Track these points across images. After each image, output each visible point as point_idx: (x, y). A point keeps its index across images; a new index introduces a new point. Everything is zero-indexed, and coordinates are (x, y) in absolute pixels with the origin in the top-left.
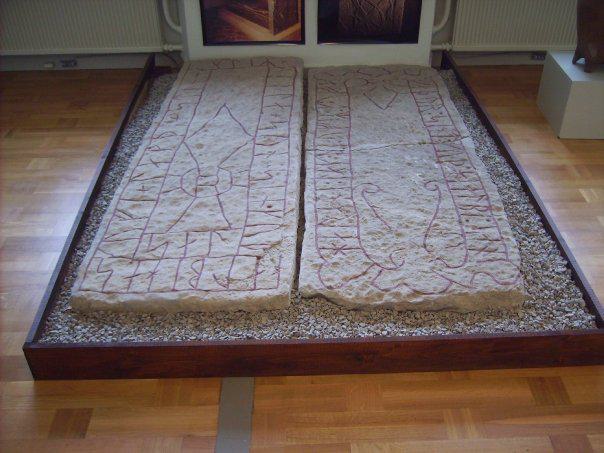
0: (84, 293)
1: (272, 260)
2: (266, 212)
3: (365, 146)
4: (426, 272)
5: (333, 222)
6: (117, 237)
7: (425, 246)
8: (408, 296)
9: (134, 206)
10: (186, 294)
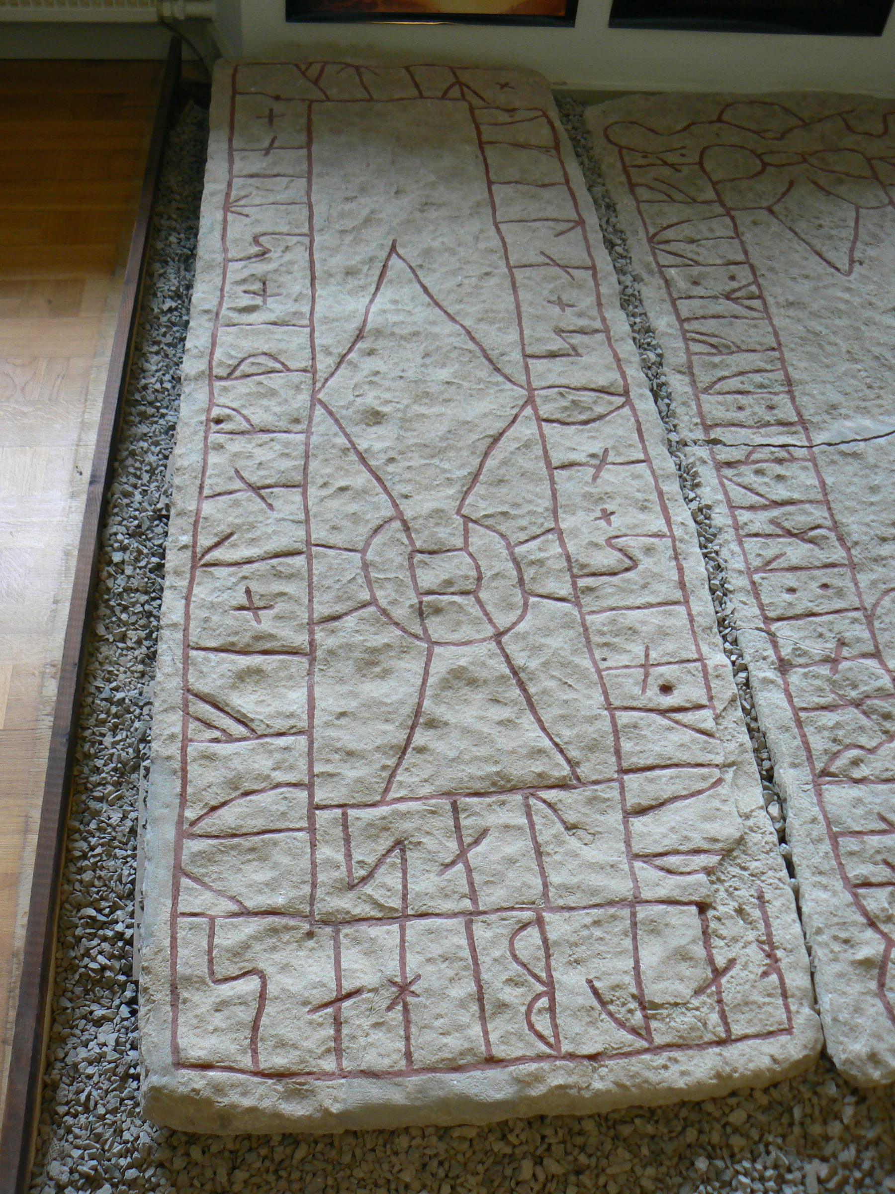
0: (197, 1081)
1: (740, 911)
5: (856, 763)
6: (228, 817)
9: (242, 677)
10: (537, 1078)
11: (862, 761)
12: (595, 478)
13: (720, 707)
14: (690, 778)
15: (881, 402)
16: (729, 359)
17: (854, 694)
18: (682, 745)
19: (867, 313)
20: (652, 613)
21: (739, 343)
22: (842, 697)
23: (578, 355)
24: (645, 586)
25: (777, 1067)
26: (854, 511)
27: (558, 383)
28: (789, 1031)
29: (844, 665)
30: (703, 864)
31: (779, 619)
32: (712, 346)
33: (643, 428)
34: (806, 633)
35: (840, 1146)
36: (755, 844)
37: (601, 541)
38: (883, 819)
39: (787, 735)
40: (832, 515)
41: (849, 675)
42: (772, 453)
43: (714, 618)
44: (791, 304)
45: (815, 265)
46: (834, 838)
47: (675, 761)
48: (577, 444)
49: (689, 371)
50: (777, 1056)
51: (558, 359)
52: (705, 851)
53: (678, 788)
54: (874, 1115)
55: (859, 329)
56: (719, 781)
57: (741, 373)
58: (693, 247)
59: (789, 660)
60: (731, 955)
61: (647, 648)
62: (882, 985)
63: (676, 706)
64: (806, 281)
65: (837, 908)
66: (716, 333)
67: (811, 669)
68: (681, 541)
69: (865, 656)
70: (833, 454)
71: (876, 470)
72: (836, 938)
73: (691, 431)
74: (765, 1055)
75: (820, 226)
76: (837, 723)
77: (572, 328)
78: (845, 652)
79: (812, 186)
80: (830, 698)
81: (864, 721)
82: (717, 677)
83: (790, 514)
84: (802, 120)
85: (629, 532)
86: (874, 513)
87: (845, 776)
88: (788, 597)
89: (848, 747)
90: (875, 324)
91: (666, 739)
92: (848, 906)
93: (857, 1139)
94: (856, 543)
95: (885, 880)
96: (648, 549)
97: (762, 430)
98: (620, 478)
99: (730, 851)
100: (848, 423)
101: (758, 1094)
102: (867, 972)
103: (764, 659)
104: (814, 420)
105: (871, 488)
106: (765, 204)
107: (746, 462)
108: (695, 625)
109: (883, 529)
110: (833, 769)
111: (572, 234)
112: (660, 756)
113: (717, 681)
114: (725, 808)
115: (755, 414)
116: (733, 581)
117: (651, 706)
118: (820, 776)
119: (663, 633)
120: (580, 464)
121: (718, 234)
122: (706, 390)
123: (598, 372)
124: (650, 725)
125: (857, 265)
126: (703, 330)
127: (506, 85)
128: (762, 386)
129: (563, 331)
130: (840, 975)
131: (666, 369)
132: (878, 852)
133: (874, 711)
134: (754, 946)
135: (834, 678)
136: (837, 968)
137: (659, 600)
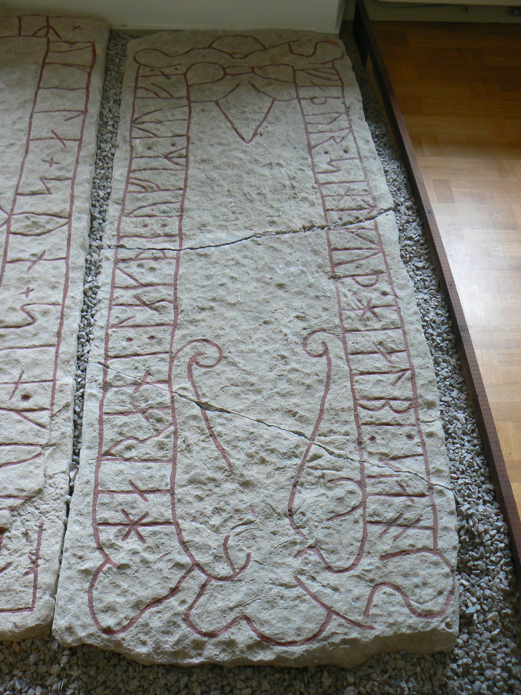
1: (26, 535)
2: (19, 411)
3: (207, 238)
4: (287, 586)
5: (129, 448)
7: (290, 513)
8: (250, 647)
11: (134, 447)
12: (30, 268)
13: (56, 409)
14: (21, 452)
15: (237, 222)
16: (149, 195)
17: (143, 405)
18: (23, 432)
19: (250, 166)
20: (33, 351)
21: (160, 185)
22: (135, 407)
23: (50, 193)
24: (35, 335)
25: (17, 630)
26: (189, 290)
27: (28, 211)
28: (31, 609)
29: (144, 387)
30: (10, 505)
31: (116, 357)
32: (143, 187)
33: (72, 238)
34: (127, 366)
35: (56, 679)
36: (49, 494)
37: (18, 307)
38: (132, 484)
39: (91, 429)
40: (175, 293)
41: (145, 394)
42: (153, 254)
43: (75, 354)
44: (203, 161)
45: (231, 136)
46: (96, 493)
47: (15, 441)
48: (28, 248)
49: (122, 202)
50: (18, 624)
51: (36, 196)
52: (15, 497)
53: (11, 458)
54: (80, 663)
55: (241, 176)
56: (40, 454)
57: (154, 204)
58: (159, 126)
59: (110, 383)
60: (9, 561)
61: (23, 372)
62: (92, 586)
63: (28, 408)
64: (219, 147)
65: (82, 537)
66: (148, 179)
67: (121, 389)
68: (68, 308)
69: (160, 382)
70: (193, 255)
71: (216, 265)
72: (74, 555)
73: (110, 240)
74: (10, 622)
75: (244, 112)
76: (125, 423)
77: (52, 177)
78: (149, 379)
79: (250, 87)
80: (128, 407)
81: (144, 423)
82: (61, 391)
83: (148, 292)
84: (263, 46)
85: (38, 302)
86: (203, 292)
87: (120, 456)
88: (125, 343)
89: (128, 438)
90: (254, 173)
91: (14, 428)
92: (89, 536)
93: (69, 676)
94: (182, 311)
95: (118, 521)
96: (45, 313)
97: (153, 240)
98: (45, 269)
99: (30, 498)
100: (209, 236)
101: (15, 645)
102: (86, 577)
103: (96, 381)
104: (187, 234)
105: (207, 276)
106: (215, 98)
107: (137, 258)
108: (59, 359)
109: (205, 302)
110: (113, 451)
111: (76, 120)
112: (6, 437)
113: (60, 394)
114: (36, 472)
115: (152, 229)
116: (95, 333)
117: (12, 407)
118: (104, 455)
119: (35, 363)
120: (23, 260)
121: (177, 118)
122: (128, 215)
123: (57, 204)
124: (7, 419)
125: (258, 136)
126: (141, 177)
127: (78, 27)
128: (164, 212)
129: (46, 179)
130: (69, 578)
131: (109, 202)
132: (120, 504)
133: (152, 416)
134: (26, 557)
135: (134, 395)
136: (69, 573)
137: (41, 343)
